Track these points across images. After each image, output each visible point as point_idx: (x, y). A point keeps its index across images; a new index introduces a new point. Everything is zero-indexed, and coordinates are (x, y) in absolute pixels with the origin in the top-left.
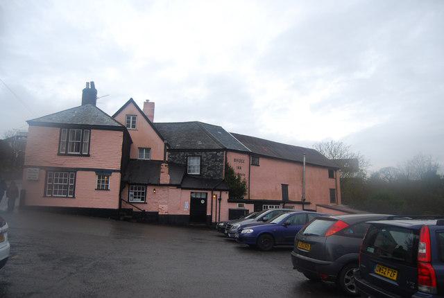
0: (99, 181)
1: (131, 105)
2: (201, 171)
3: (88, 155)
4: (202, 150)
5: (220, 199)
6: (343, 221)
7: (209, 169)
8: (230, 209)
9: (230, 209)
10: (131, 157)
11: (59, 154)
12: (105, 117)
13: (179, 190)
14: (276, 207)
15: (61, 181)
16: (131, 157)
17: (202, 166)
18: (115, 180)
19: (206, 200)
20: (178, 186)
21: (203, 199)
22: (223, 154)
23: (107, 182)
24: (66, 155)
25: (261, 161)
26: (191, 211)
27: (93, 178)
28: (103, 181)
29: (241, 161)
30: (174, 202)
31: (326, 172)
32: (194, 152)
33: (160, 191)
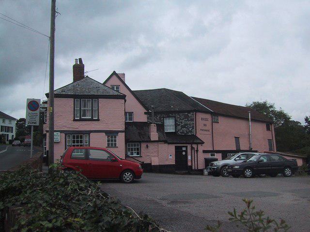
0: (108, 141)
2: (176, 129)
3: (98, 120)
4: (175, 112)
5: (197, 151)
6: (288, 161)
7: (182, 127)
8: (222, 159)
9: (222, 159)
11: (74, 120)
12: (100, 85)
13: (166, 145)
15: (78, 142)
17: (176, 125)
18: (121, 139)
19: (186, 151)
20: (165, 142)
21: (184, 151)
23: (115, 141)
24: (81, 120)
26: (176, 161)
28: (112, 140)
29: (206, 120)
30: (164, 154)
32: (169, 114)
33: (151, 146)
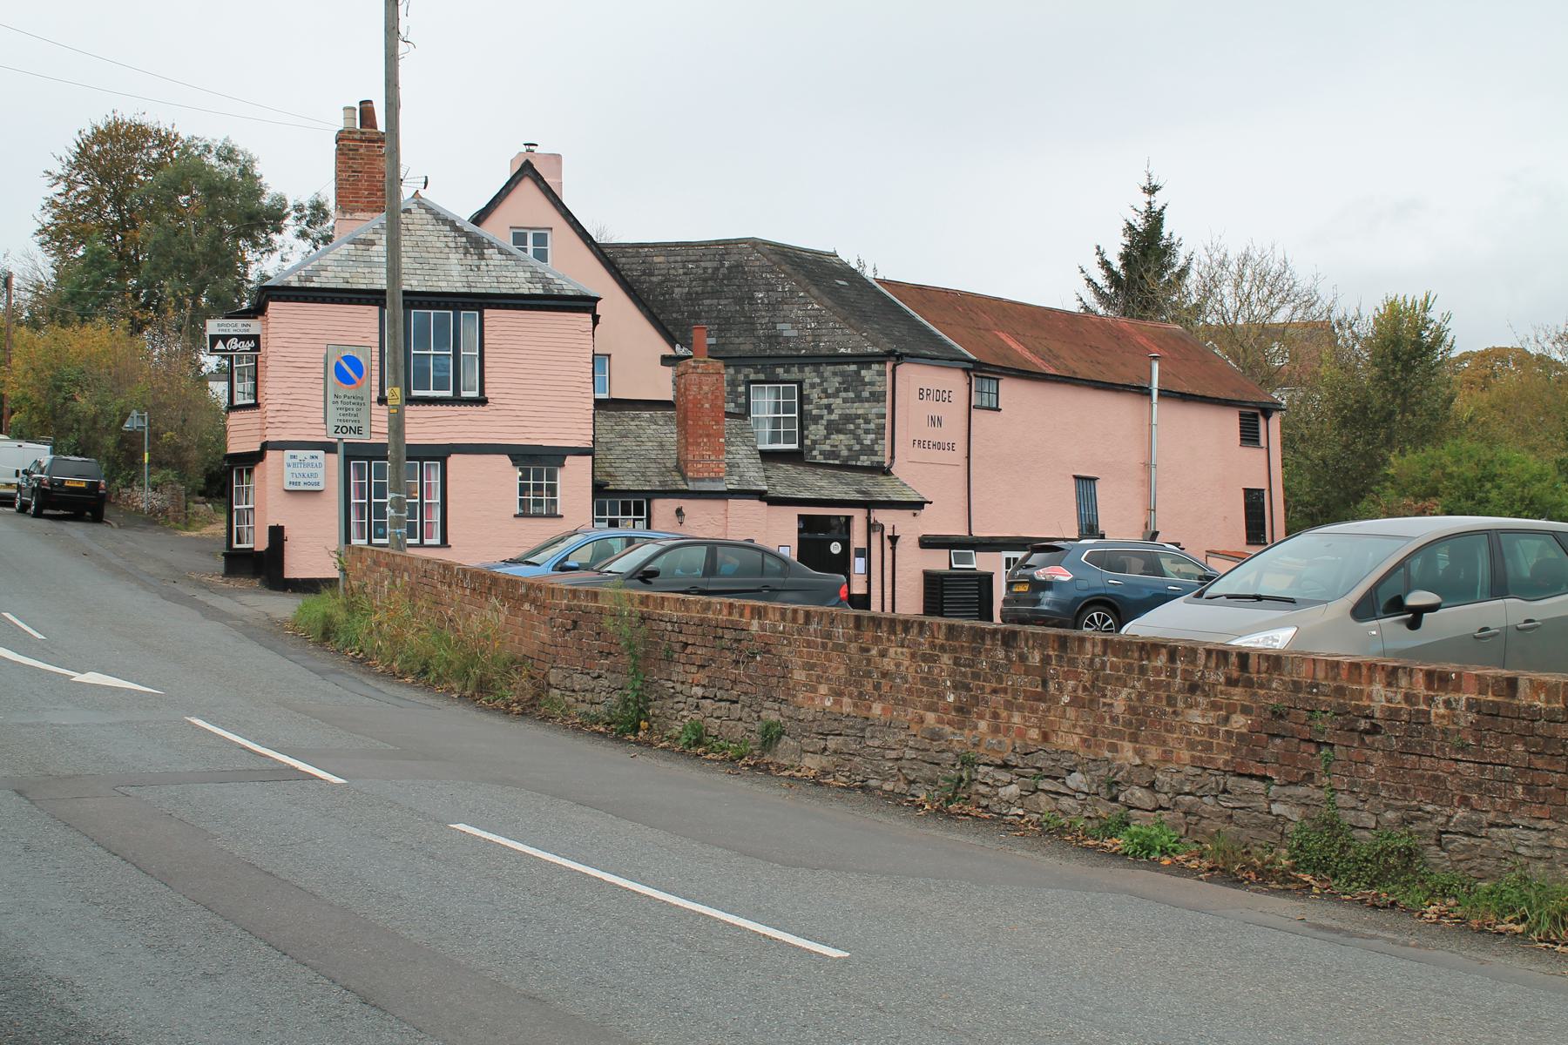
1: (527, 186)
3: (482, 401)
7: (833, 428)
10: (286, 577)
14: (1512, 684)
16: (286, 577)
18: (574, 480)
22: (882, 374)
23: (552, 490)
25: (1011, 391)
27: (506, 474)
28: (538, 488)
29: (942, 396)
31: (1230, 422)
